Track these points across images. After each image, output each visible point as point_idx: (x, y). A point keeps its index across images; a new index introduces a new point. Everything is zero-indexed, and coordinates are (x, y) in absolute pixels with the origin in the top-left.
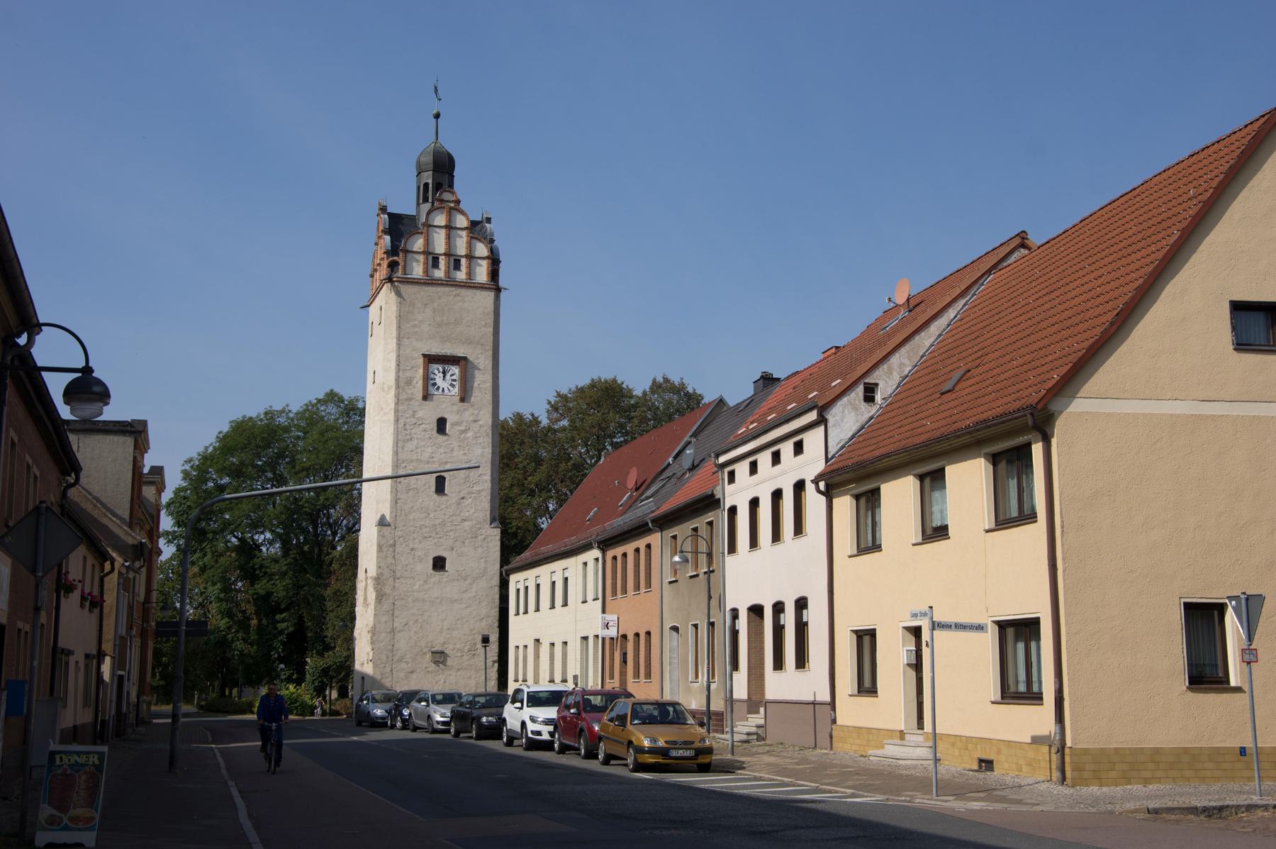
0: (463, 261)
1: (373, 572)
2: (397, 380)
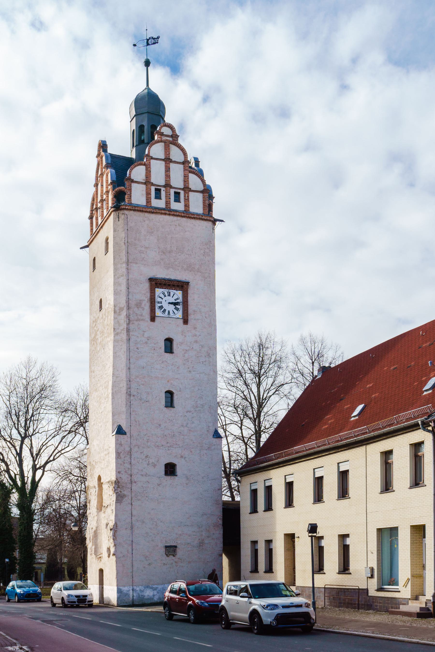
0: (182, 193)
2: (128, 302)
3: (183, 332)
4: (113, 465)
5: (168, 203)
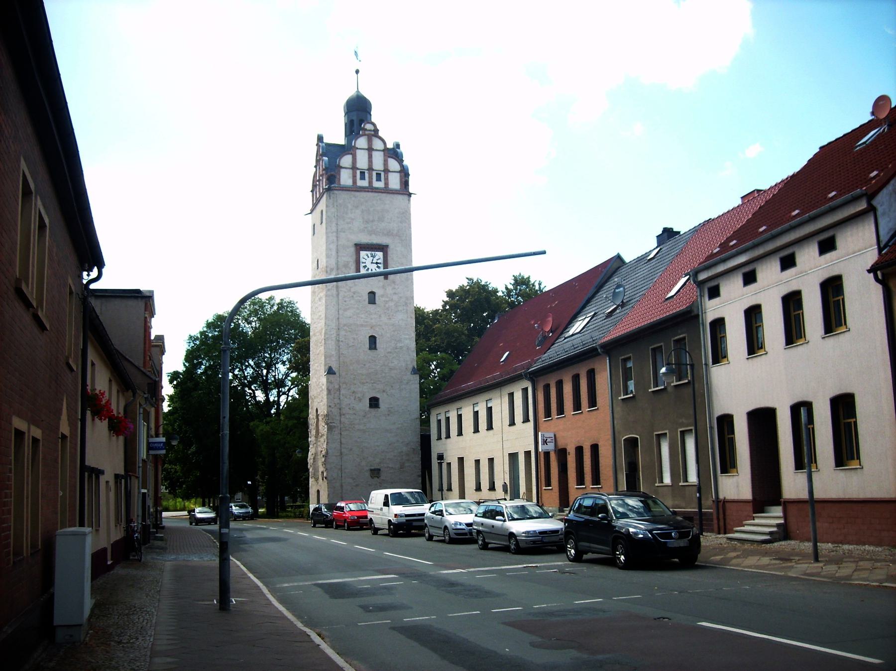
0: (383, 174)
1: (323, 411)
2: (337, 264)
3: (383, 287)
4: (325, 400)
5: (370, 182)
